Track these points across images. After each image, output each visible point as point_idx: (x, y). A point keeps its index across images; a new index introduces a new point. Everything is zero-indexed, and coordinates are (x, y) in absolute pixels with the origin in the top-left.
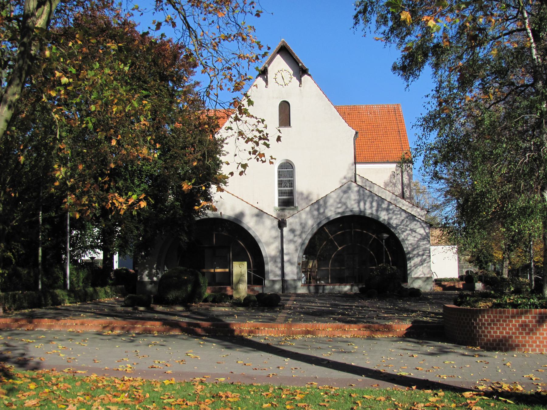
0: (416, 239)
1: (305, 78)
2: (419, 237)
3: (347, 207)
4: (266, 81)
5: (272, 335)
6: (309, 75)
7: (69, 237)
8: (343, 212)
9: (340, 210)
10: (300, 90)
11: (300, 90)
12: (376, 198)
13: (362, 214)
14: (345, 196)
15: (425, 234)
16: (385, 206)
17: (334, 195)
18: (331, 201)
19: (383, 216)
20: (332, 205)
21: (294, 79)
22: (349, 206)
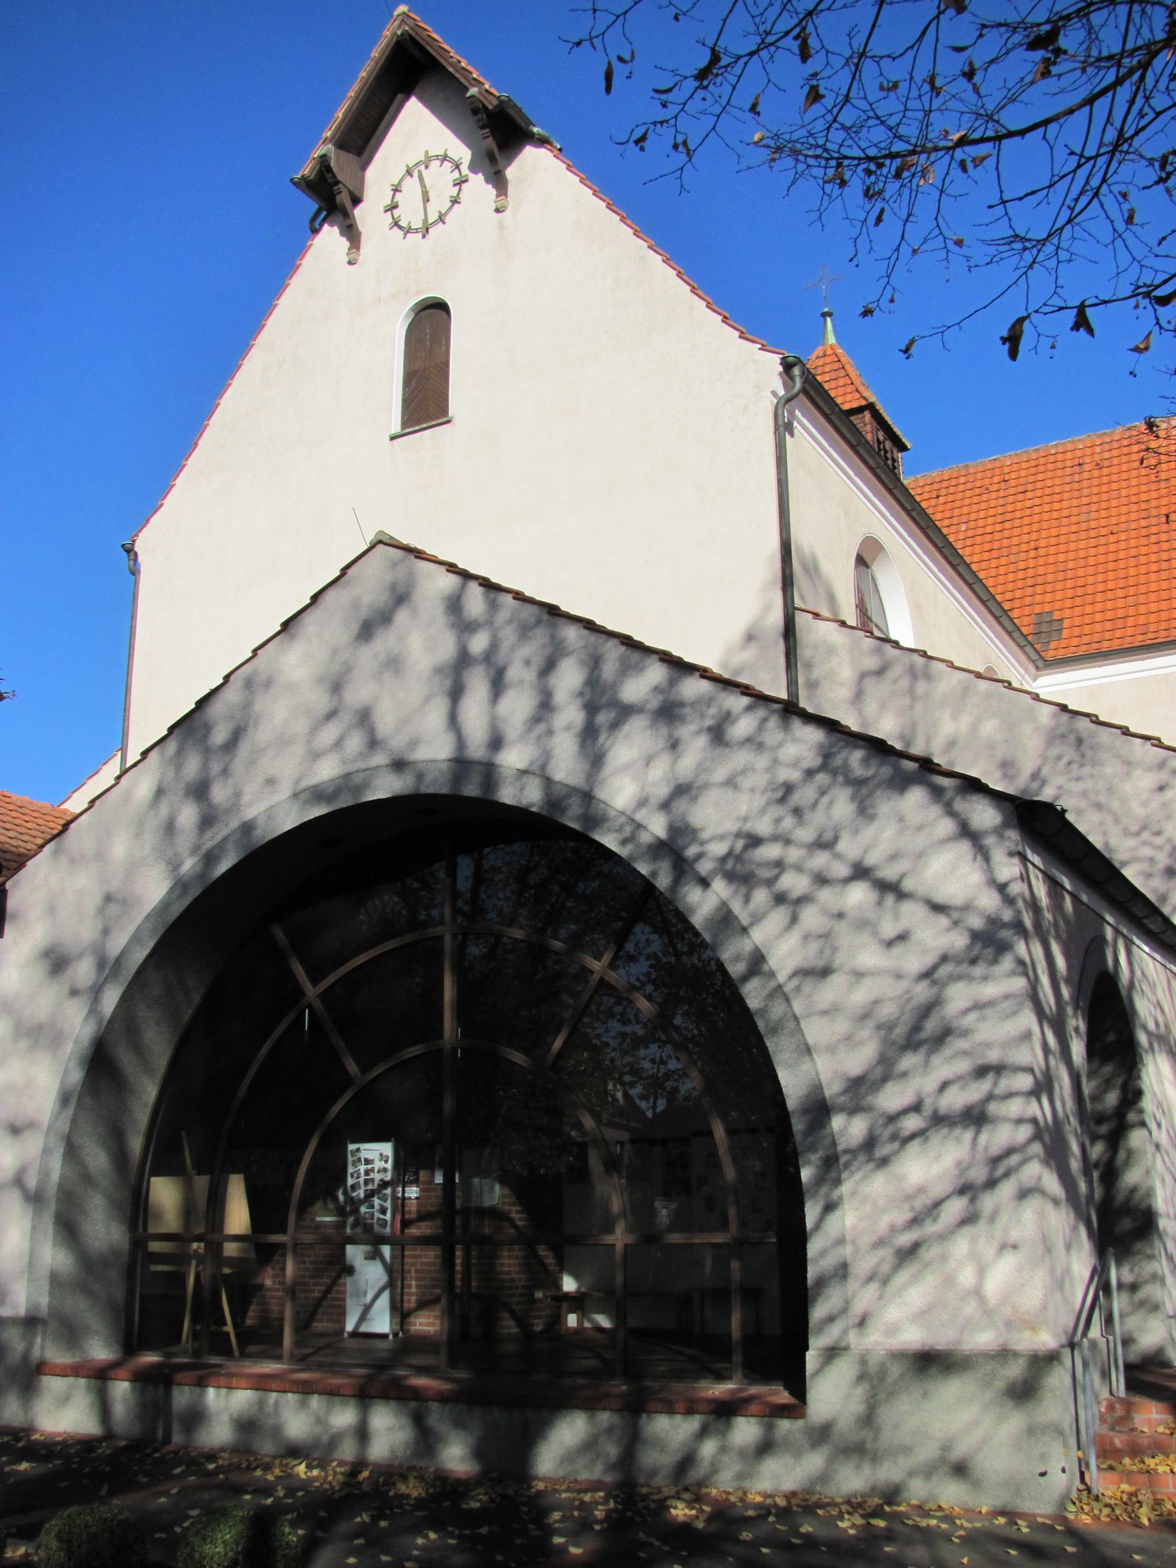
0: (913, 961)
1: (534, 165)
2: (935, 938)
3: (373, 743)
4: (351, 232)
5: (474, 1284)
6: (542, 142)
7: (1068, 885)
8: (345, 783)
9: (327, 771)
10: (501, 226)
11: (501, 226)
12: (572, 634)
13: (471, 790)
14: (368, 656)
15: (989, 901)
16: (641, 686)
17: (298, 664)
18: (278, 715)
19: (631, 786)
20: (283, 742)
21: (477, 181)
22: (386, 721)
